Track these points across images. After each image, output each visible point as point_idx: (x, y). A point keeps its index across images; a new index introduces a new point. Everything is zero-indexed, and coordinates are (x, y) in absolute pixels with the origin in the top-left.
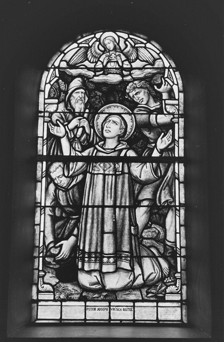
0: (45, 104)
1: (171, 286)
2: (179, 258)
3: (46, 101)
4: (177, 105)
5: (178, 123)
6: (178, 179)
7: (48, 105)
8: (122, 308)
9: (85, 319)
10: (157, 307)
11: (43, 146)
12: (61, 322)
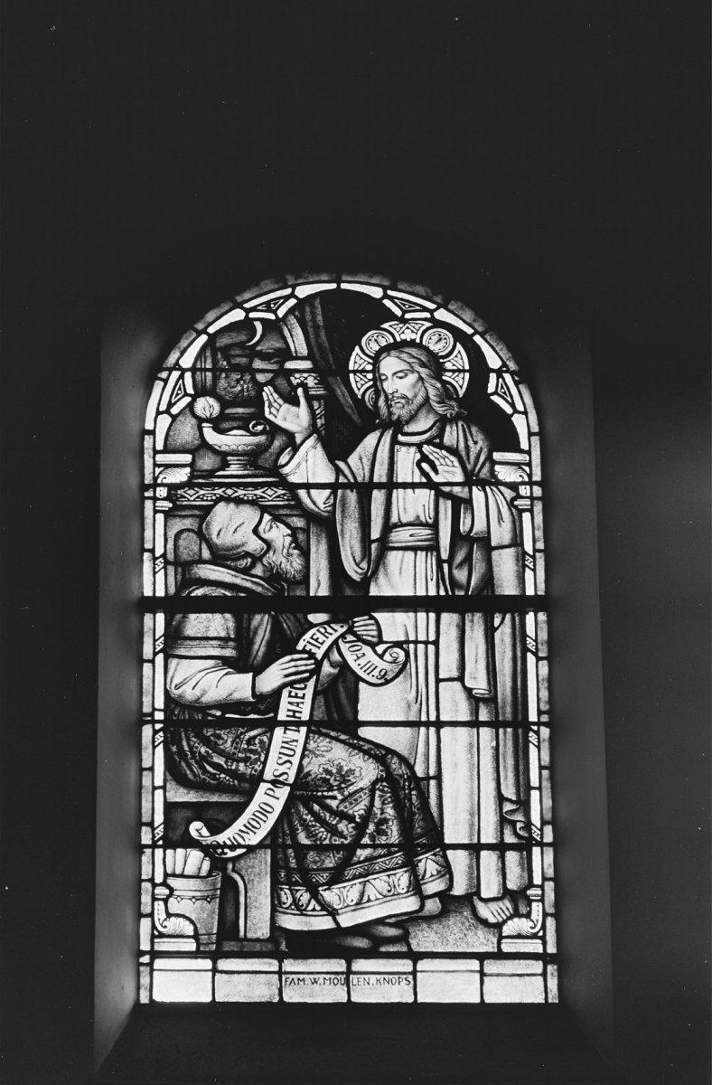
0: (155, 465)
5: (531, 511)
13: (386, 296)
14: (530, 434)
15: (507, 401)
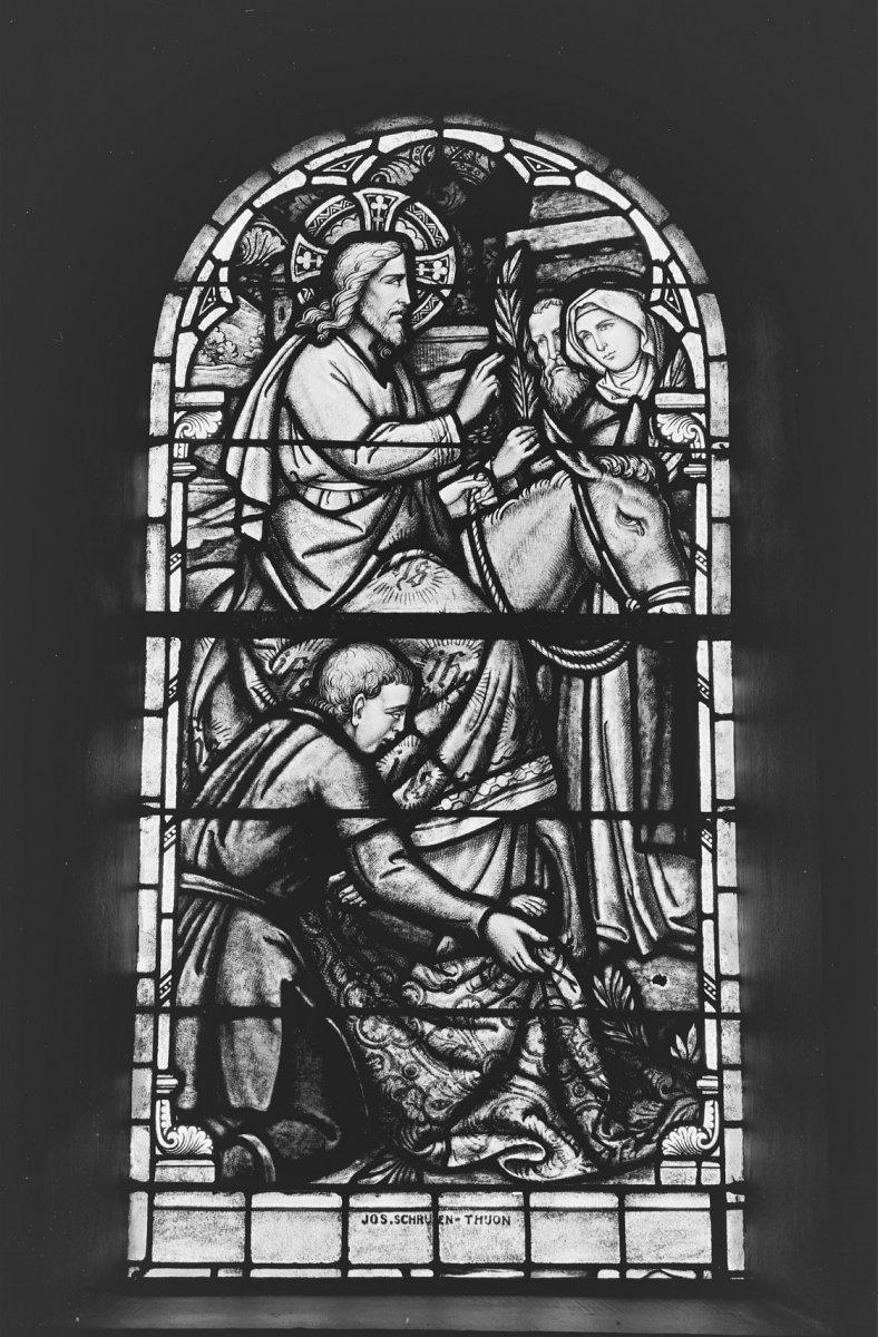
1: (682, 1129)
2: (714, 1022)
3: (182, 399)
4: (700, 411)
5: (707, 479)
6: (710, 703)
7: (186, 415)
9: (248, 1265)
11: (168, 573)
12: (247, 1273)
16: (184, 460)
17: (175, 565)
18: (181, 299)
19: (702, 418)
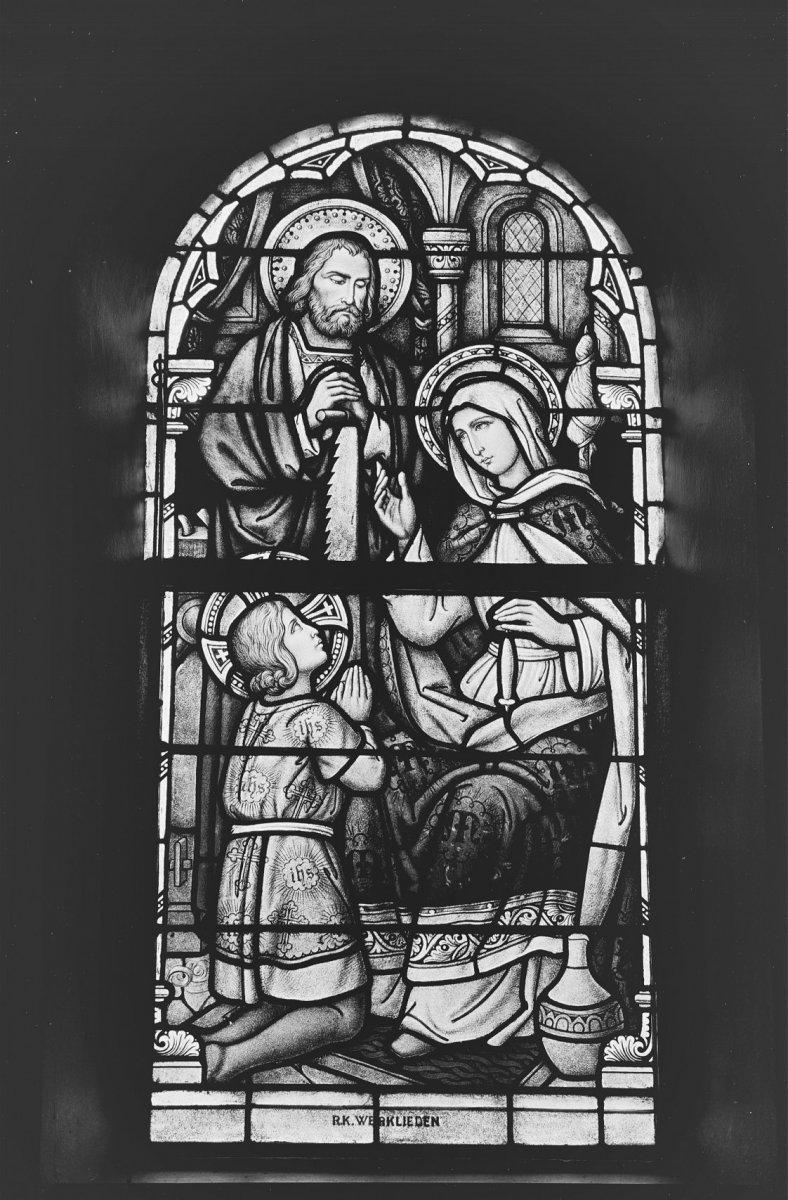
4: (636, 383)
5: (643, 445)
8: (351, 1114)
10: (249, 1107)
13: (466, 149)
14: (643, 342)
15: (614, 299)
16: (177, 420)
17: (169, 513)
18: (253, 1139)
19: (638, 389)
